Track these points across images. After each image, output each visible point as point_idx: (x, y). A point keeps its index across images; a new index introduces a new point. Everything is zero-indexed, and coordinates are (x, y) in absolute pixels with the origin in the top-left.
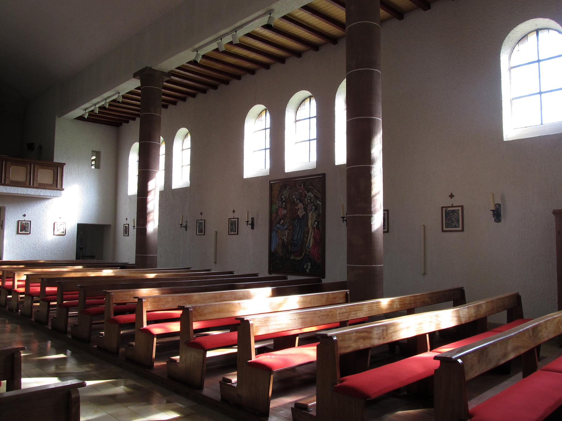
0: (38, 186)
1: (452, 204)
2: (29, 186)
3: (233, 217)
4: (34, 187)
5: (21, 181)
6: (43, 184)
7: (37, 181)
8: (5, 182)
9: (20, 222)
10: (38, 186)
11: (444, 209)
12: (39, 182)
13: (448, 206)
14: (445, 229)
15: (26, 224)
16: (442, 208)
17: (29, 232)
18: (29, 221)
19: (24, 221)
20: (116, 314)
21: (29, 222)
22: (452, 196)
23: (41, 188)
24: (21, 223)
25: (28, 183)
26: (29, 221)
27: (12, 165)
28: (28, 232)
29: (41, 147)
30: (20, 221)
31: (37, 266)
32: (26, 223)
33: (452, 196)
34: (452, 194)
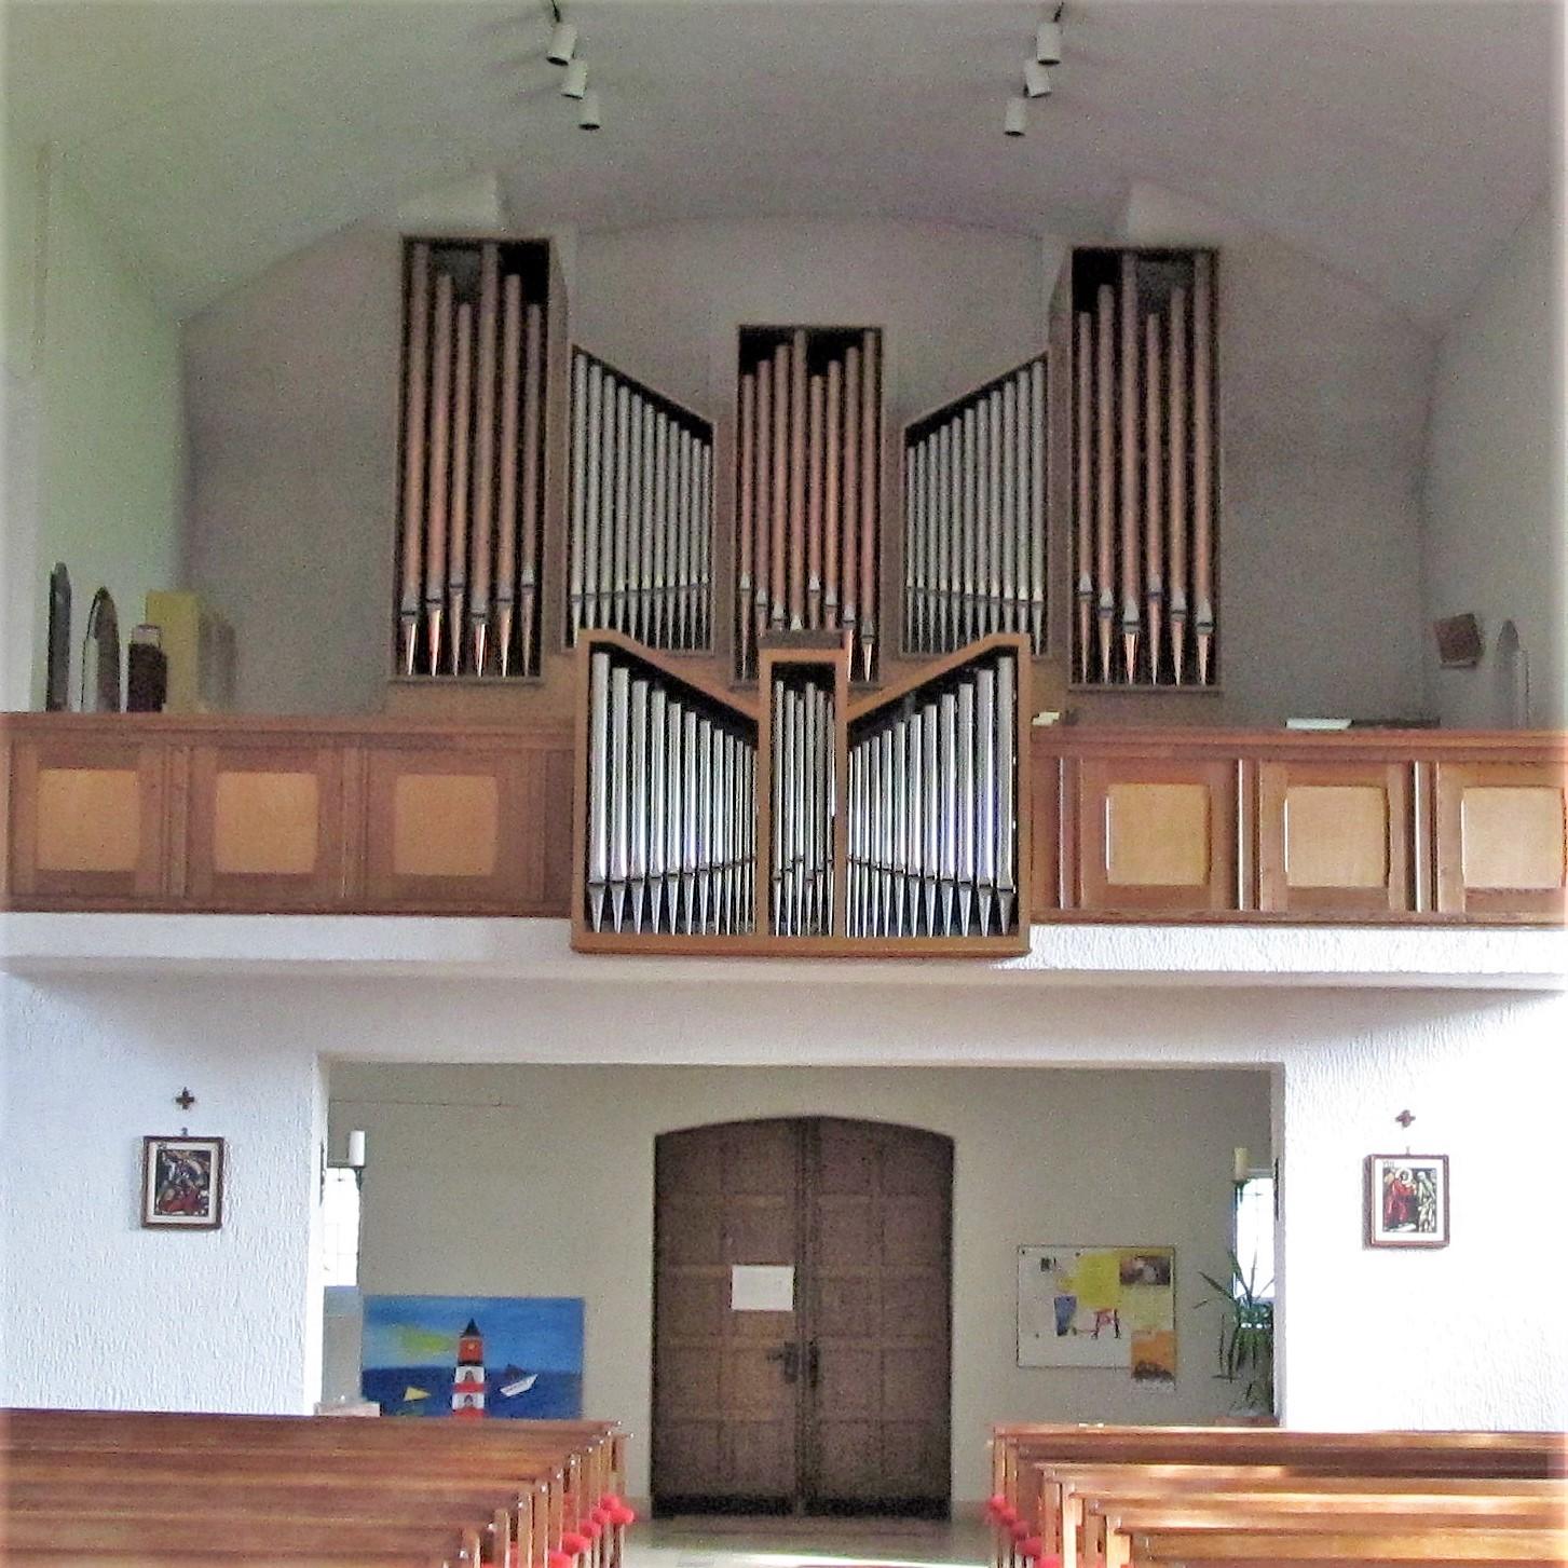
0: (1282, 906)
1: (185, 1130)
2: (1230, 916)
3: (179, 1134)
4: (1436, 921)
5: (1354, 883)
6: (1499, 892)
7: (1456, 873)
8: (1256, 904)
9: (1379, 1165)
10: (1282, 906)
11: (154, 1147)
12: (1468, 883)
13: (170, 1135)
14: (210, 1219)
15: (1416, 1179)
16: (149, 1139)
17: (1439, 1236)
18: (1432, 1157)
19: (1408, 1156)
20: (284, 1396)
21: (1438, 1165)
22: (1405, 1119)
23: (1484, 925)
24: (1386, 1171)
25: (1396, 900)
26: (1432, 1157)
27: (1290, 783)
28: (1434, 1230)
29: (1510, 632)
30: (1378, 1156)
31: (1394, 1474)
32: (1416, 1172)
33: (1405, 1119)
34: (185, 1093)
